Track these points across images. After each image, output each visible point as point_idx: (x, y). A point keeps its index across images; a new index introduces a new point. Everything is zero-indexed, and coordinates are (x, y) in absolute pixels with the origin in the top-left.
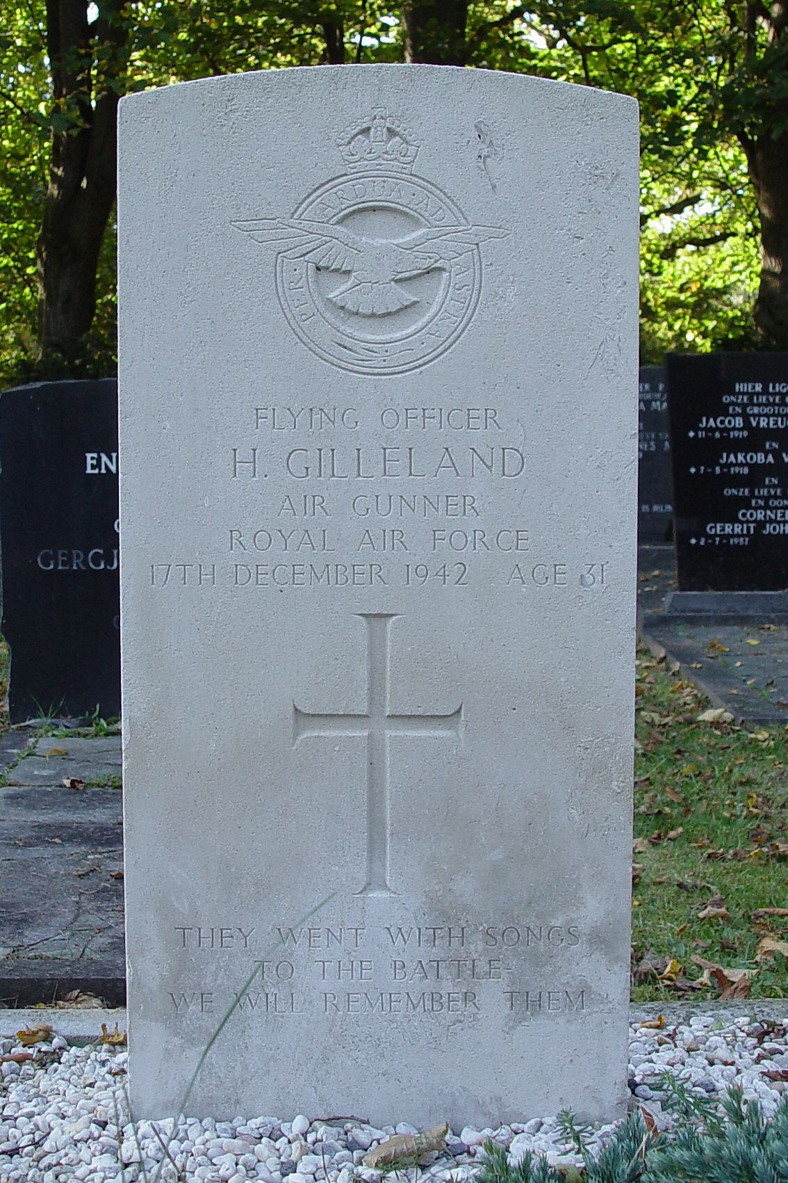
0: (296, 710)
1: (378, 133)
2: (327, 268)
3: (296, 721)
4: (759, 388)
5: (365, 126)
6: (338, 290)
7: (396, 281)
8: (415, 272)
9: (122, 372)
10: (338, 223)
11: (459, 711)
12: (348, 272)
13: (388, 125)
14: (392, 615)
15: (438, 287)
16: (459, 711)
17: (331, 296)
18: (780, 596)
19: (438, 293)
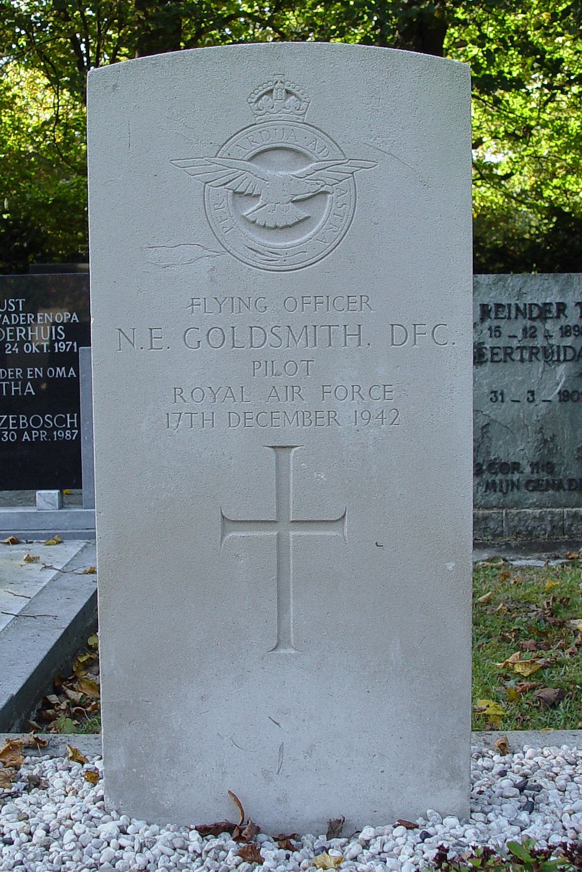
0: (223, 517)
1: (278, 94)
2: (242, 193)
3: (224, 525)
5: (269, 88)
6: (250, 210)
7: (293, 202)
8: (308, 195)
9: (93, 258)
11: (343, 517)
15: (324, 208)
16: (343, 517)
17: (245, 214)
19: (324, 210)
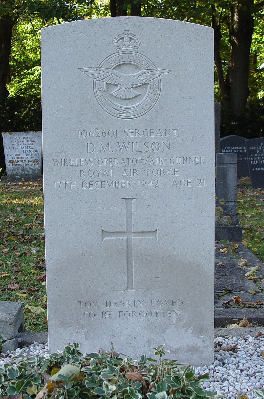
0: (103, 230)
1: (127, 39)
4: (229, 148)
6: (114, 91)
7: (133, 88)
10: (114, 69)
12: (117, 85)
13: (130, 36)
14: (134, 199)
18: (123, 240)
19: (147, 95)
